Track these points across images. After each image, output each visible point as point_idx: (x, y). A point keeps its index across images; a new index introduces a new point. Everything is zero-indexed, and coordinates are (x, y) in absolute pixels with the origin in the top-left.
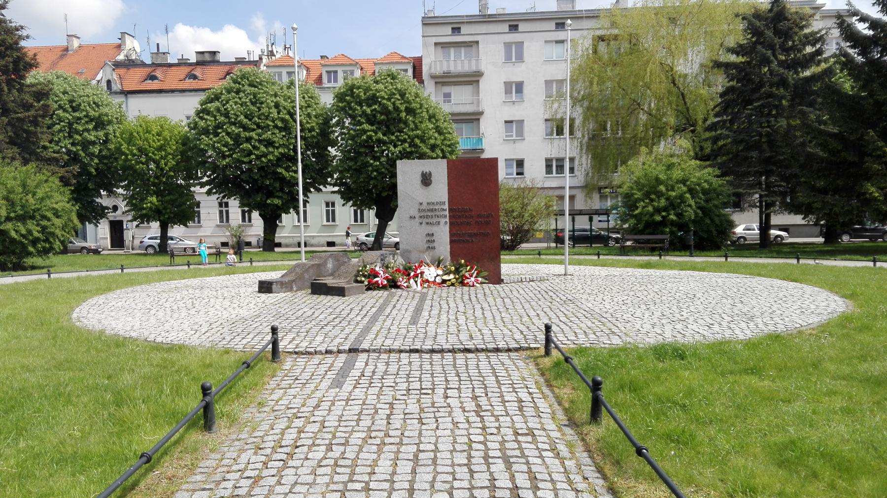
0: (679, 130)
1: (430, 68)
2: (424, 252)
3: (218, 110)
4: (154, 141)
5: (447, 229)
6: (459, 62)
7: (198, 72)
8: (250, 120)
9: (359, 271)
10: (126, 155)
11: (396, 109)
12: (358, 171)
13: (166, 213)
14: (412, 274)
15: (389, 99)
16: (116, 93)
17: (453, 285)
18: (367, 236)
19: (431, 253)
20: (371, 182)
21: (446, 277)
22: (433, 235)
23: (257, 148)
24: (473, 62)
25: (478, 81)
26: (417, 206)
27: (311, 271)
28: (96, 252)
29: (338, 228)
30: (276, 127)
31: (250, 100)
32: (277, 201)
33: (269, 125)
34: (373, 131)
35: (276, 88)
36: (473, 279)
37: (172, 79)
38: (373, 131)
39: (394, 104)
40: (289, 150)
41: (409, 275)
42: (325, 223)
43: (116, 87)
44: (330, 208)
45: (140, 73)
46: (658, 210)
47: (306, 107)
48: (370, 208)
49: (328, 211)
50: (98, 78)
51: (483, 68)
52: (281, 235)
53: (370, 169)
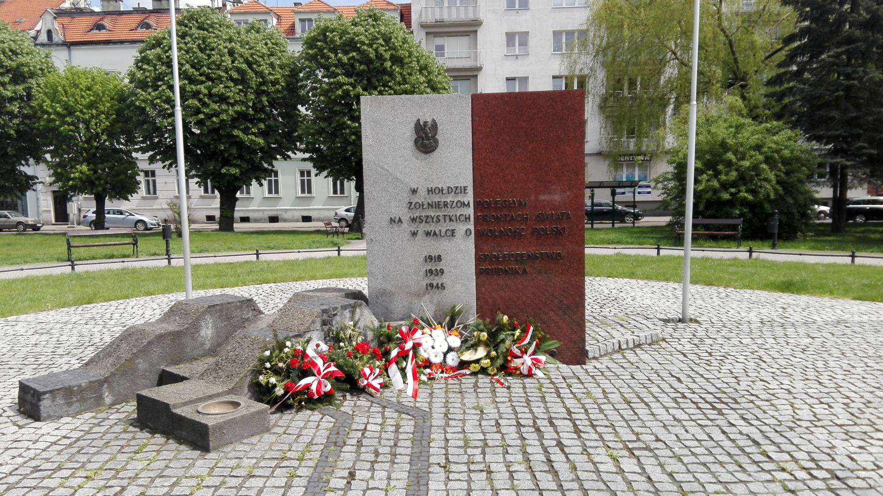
0: (728, 86)
1: (420, 16)
2: (419, 296)
3: (159, 58)
4: (82, 97)
5: (469, 246)
6: (454, 9)
7: (152, 21)
8: (197, 70)
9: (262, 361)
10: (49, 114)
11: (379, 57)
12: (334, 135)
13: (100, 185)
14: (394, 353)
15: (370, 45)
16: (58, 45)
17: (483, 371)
18: (347, 210)
19: (437, 296)
20: (349, 148)
21: (468, 356)
22: (439, 258)
23: (207, 106)
24: (471, 9)
25: (476, 32)
26: (406, 197)
27: (156, 351)
28: (35, 228)
29: (314, 201)
30: (231, 79)
31: (199, 45)
32: (234, 171)
33: (220, 77)
34: (350, 84)
35: (231, 32)
36: (528, 359)
37: (121, 29)
38: (350, 84)
39: (376, 50)
40: (248, 107)
41: (387, 353)
42: (300, 195)
43: (58, 37)
44: (306, 178)
45: (85, 22)
46: (725, 186)
47: (269, 56)
48: (349, 179)
49: (302, 182)
50: (38, 28)
51: (481, 16)
52: (240, 210)
53: (348, 131)
